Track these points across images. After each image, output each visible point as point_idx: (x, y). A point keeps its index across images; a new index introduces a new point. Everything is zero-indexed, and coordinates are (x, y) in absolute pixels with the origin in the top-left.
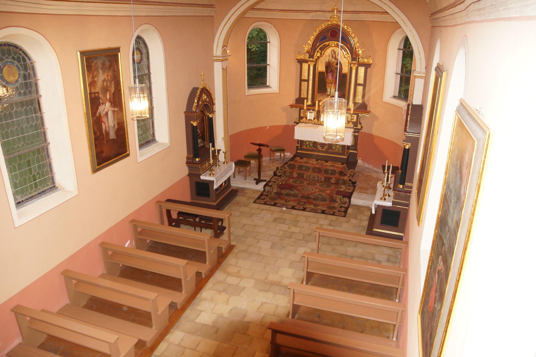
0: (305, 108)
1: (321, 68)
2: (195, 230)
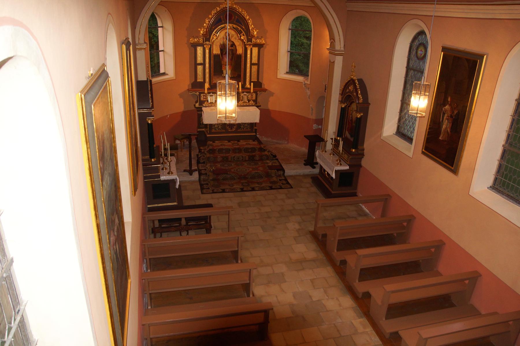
0: (206, 92)
1: (216, 51)
2: (181, 235)
